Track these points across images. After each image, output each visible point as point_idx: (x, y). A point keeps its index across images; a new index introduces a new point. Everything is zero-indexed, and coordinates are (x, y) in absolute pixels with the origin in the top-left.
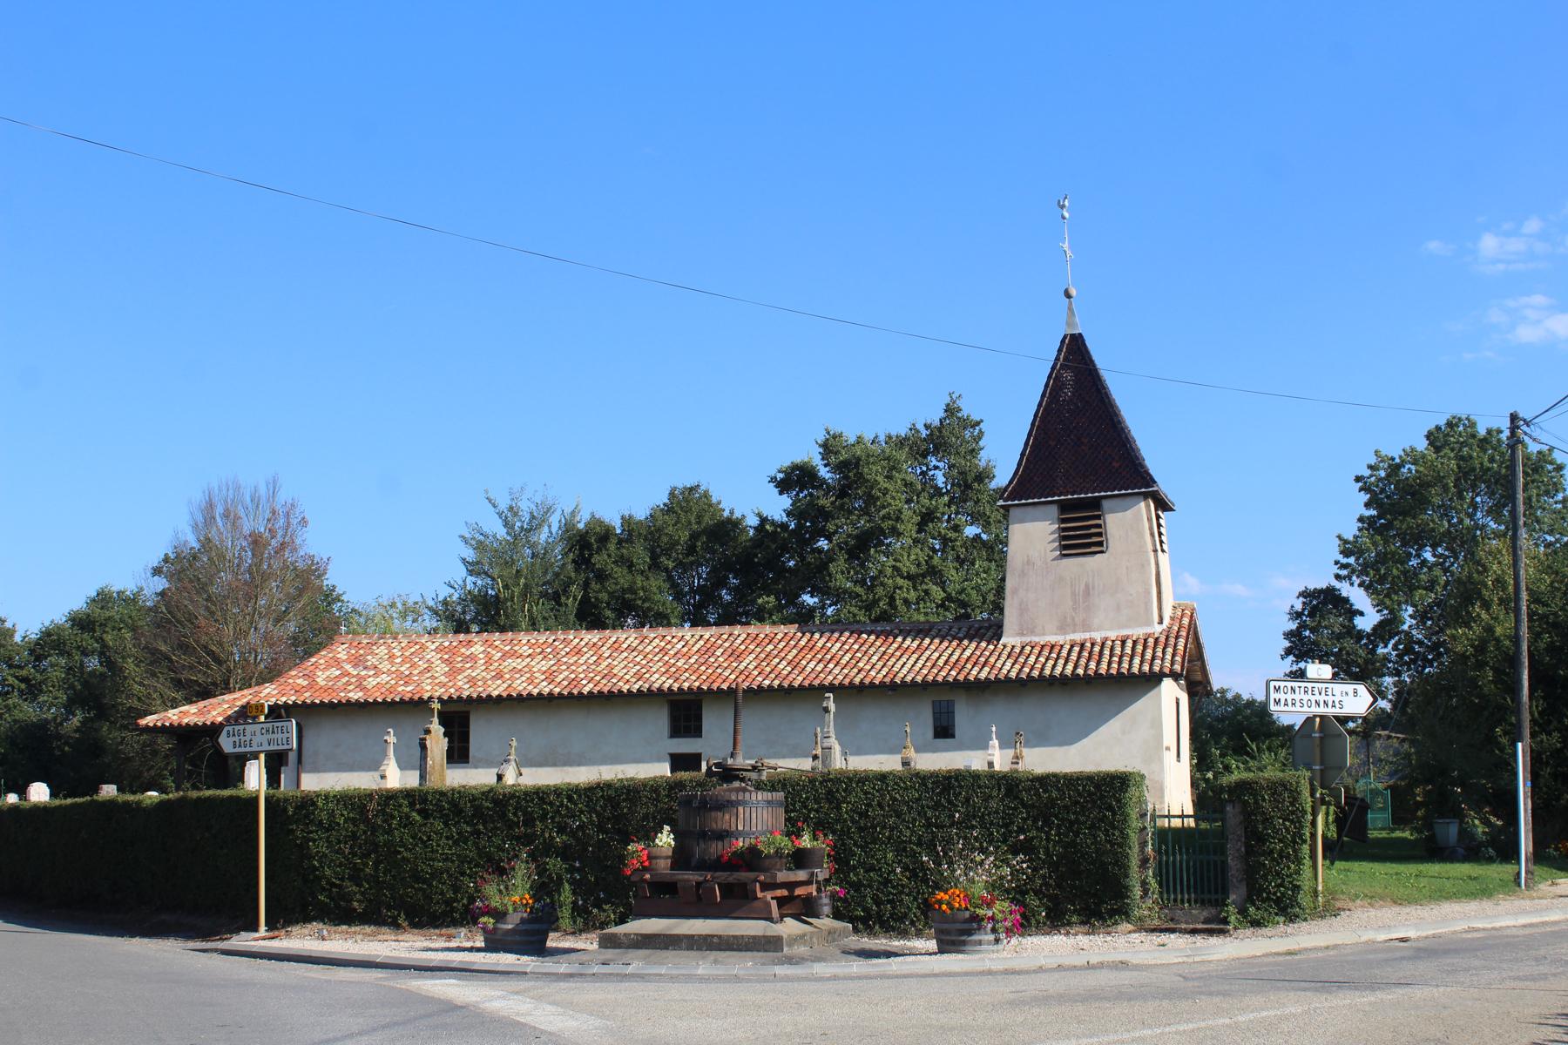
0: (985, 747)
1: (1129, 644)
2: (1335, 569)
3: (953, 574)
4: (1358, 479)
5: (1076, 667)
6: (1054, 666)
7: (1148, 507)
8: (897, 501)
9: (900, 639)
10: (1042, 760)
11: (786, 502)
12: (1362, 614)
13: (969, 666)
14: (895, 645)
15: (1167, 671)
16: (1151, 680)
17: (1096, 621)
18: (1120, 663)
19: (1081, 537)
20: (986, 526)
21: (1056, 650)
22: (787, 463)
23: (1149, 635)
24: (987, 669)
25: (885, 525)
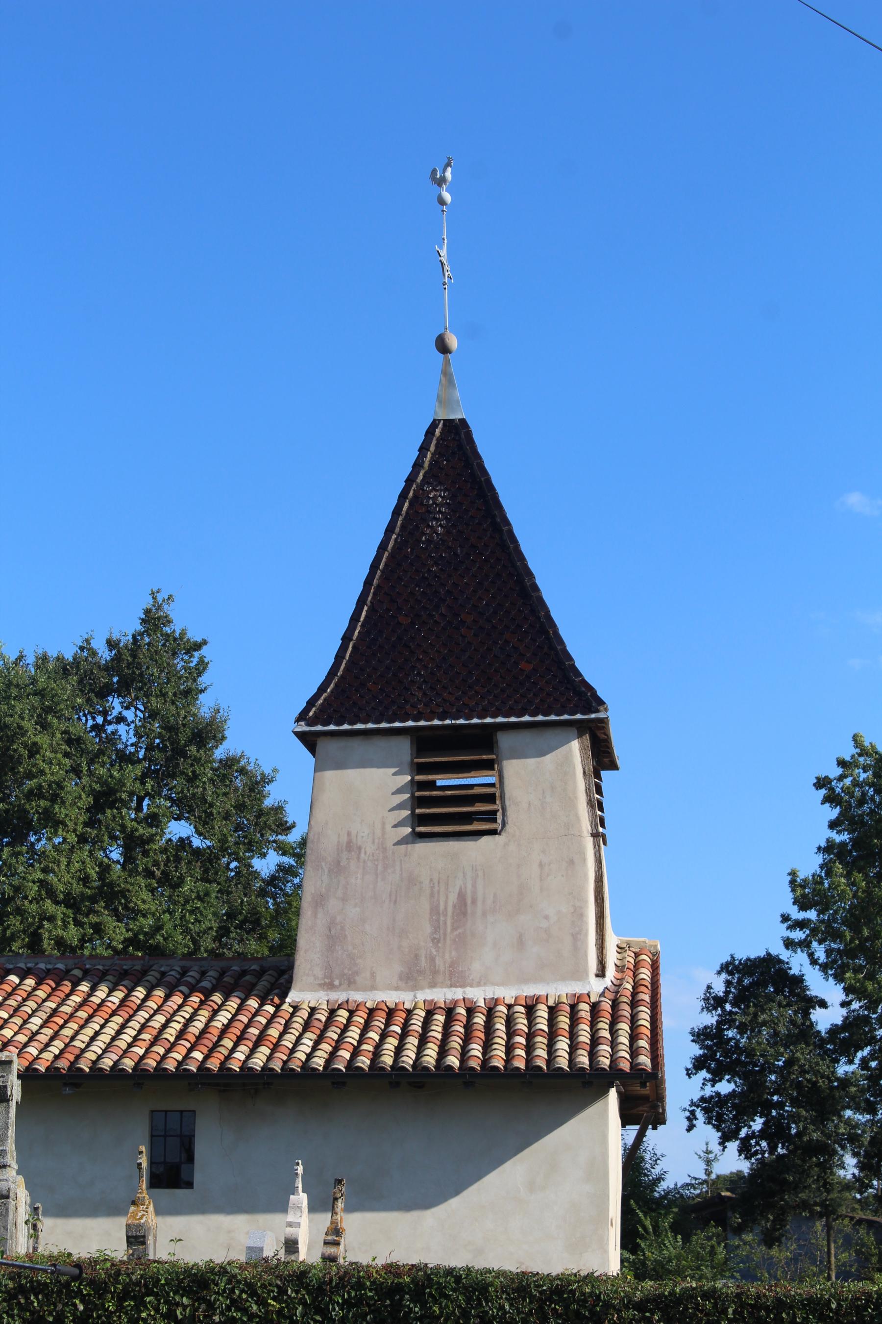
0: (282, 1207)
1: (542, 1012)
2: (782, 931)
3: (142, 897)
4: (821, 783)
5: (443, 1052)
6: (399, 1051)
8: (53, 765)
9: (84, 987)
10: (385, 1239)
12: (823, 1004)
13: (228, 1043)
14: (76, 999)
17: (476, 968)
18: (530, 1048)
20: (204, 825)
21: (400, 1018)
24: (264, 1051)
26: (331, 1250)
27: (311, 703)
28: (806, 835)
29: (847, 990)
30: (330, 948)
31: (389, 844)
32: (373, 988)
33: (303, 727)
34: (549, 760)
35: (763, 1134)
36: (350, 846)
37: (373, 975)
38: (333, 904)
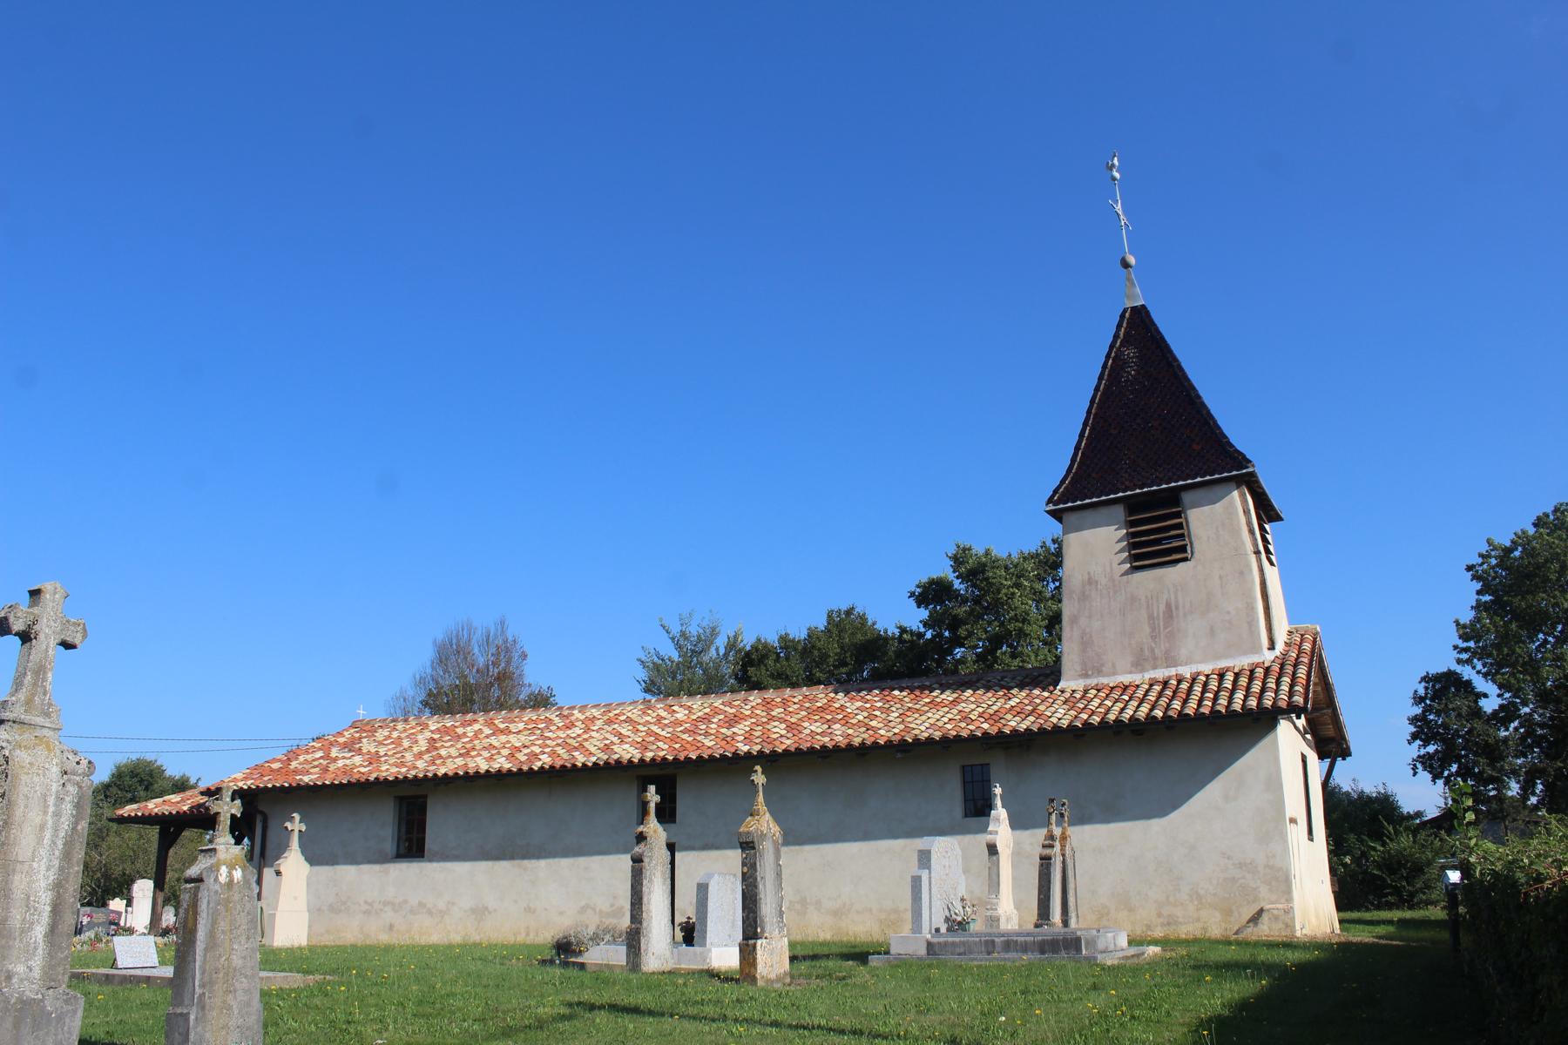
1: (1230, 677)
2: (1455, 654)
4: (1469, 568)
5: (1153, 708)
6: (1122, 710)
7: (1243, 496)
11: (924, 614)
12: (1486, 696)
15: (1283, 704)
16: (1261, 721)
18: (1215, 700)
19: (1157, 542)
22: (925, 580)
23: (1257, 665)
25: (1011, 627)
26: (1047, 851)
27: (1055, 492)
28: (1463, 599)
29: (1500, 687)
30: (1084, 651)
31: (1117, 576)
32: (1114, 674)
33: (1051, 507)
34: (1218, 507)
35: (1458, 773)
36: (1091, 581)
37: (1114, 666)
38: (1083, 621)
